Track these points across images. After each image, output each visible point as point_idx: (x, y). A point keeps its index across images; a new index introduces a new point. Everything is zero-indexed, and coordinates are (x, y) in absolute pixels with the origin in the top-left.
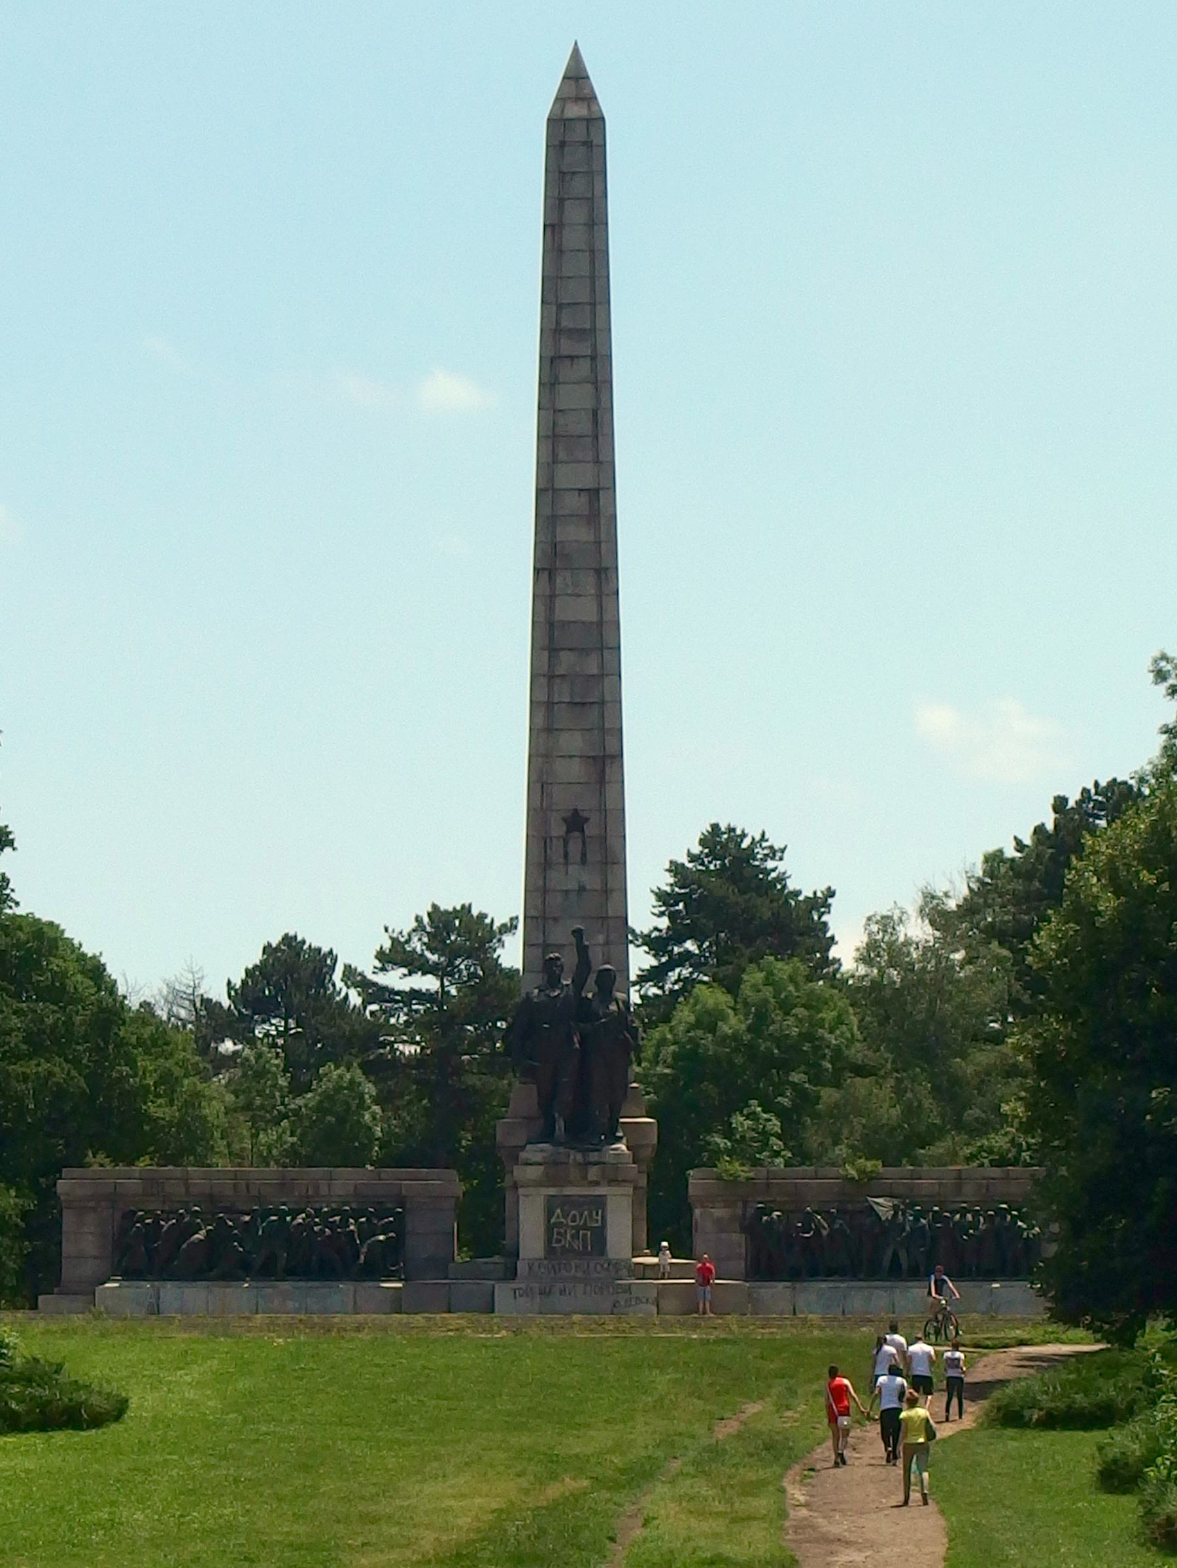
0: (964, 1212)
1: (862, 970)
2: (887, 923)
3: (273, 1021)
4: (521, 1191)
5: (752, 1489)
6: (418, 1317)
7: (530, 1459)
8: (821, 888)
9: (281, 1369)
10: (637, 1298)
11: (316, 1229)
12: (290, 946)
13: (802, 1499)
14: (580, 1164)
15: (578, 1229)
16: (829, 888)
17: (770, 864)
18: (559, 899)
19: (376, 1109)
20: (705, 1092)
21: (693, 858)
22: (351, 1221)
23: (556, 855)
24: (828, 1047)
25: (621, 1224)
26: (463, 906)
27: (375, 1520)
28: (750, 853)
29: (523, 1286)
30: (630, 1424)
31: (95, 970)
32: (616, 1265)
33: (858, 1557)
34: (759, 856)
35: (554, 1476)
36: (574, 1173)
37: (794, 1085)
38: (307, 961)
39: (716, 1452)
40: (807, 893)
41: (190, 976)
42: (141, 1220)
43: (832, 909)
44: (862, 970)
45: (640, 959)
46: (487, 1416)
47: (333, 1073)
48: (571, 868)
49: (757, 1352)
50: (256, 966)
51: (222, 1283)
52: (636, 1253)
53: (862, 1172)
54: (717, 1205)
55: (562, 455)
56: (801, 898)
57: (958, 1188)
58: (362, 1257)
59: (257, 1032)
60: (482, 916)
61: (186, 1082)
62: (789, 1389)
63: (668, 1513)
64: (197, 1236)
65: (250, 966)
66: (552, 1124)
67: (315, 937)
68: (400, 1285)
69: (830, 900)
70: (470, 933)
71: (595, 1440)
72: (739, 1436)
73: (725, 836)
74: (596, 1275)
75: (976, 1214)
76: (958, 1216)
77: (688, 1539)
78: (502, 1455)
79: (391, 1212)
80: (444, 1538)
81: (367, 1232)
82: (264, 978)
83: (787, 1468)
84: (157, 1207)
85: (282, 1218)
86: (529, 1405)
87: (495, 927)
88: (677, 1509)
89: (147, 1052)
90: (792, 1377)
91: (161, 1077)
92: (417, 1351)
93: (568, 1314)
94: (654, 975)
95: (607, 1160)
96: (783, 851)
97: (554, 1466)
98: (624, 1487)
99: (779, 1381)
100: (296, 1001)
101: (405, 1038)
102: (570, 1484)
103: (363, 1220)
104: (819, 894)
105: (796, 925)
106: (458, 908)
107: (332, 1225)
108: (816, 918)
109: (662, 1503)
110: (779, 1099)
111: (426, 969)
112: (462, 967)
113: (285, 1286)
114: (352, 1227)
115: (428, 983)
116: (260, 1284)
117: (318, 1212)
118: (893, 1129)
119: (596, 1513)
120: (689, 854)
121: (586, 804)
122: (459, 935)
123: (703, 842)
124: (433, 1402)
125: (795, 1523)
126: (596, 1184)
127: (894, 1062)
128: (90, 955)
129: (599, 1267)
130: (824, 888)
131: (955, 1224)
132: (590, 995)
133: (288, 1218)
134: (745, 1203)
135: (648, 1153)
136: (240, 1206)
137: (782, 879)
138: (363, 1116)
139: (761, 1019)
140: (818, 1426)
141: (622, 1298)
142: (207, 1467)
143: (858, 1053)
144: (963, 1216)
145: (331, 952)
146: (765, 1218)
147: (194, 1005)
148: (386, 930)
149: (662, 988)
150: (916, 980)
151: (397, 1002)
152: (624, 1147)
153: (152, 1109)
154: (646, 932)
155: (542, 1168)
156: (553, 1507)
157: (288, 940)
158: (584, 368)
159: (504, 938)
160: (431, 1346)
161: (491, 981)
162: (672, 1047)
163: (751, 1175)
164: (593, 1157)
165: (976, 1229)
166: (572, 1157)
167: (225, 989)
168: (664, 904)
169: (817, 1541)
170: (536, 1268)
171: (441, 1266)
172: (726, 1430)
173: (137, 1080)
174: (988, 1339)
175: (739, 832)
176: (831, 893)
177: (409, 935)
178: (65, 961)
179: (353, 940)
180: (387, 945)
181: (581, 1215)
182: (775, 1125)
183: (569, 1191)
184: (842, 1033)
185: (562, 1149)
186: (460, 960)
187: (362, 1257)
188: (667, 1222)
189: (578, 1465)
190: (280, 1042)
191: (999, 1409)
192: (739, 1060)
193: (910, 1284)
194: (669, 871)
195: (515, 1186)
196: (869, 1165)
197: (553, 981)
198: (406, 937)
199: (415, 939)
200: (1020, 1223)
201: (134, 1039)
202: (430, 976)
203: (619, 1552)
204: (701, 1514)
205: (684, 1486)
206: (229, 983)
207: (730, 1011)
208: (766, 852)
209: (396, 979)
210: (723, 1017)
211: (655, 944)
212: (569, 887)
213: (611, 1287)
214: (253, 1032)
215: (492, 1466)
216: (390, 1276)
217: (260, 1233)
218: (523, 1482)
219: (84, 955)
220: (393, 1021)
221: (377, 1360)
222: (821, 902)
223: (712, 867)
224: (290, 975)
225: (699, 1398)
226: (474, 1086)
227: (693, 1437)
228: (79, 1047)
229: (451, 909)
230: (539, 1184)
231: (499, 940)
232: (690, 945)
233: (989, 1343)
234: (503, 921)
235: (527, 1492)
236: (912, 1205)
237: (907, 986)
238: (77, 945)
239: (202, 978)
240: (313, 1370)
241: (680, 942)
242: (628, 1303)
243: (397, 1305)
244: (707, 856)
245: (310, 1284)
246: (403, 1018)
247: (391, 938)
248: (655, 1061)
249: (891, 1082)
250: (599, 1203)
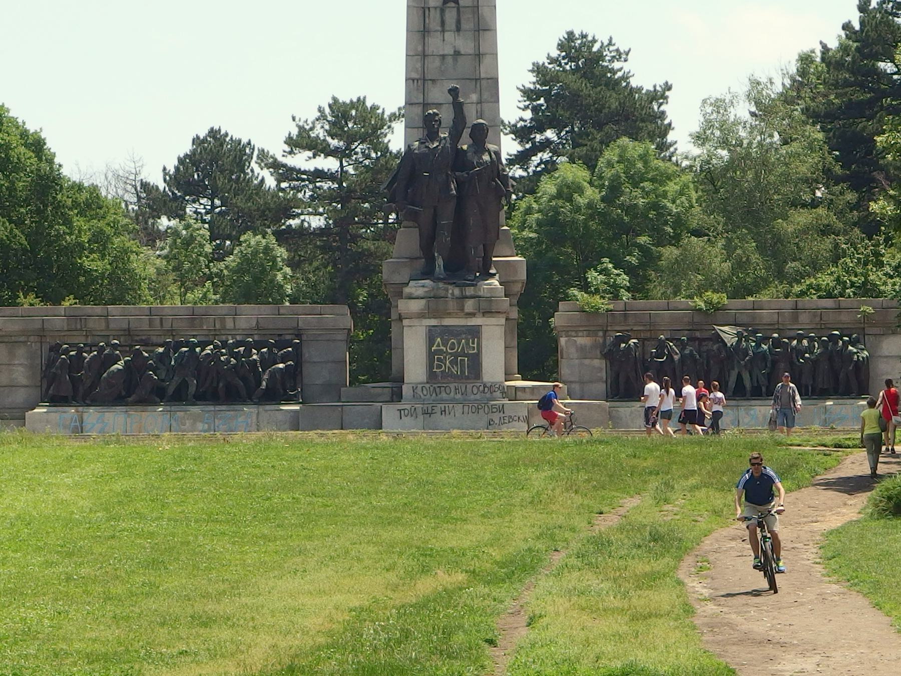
0: (800, 338)
1: (696, 151)
2: (719, 105)
3: (202, 201)
4: (406, 322)
5: (652, 580)
6: (311, 433)
7: (401, 554)
8: (660, 82)
9: (161, 471)
10: (510, 417)
11: (222, 358)
12: (214, 138)
13: (706, 592)
15: (456, 355)
16: (667, 83)
17: (616, 65)
18: (438, 62)
19: (288, 270)
20: (565, 250)
21: (553, 61)
22: (254, 351)
23: (434, 24)
24: (670, 215)
25: (495, 353)
26: (359, 99)
27: (206, 622)
28: (600, 56)
29: (408, 407)
30: (507, 519)
31: (37, 145)
32: (491, 388)
33: (809, 664)
34: (607, 58)
35: (425, 570)
36: (452, 305)
37: (640, 247)
38: (230, 150)
39: (601, 544)
40: (648, 86)
41: (132, 165)
42: (66, 352)
43: (669, 100)
44: (696, 151)
45: (509, 146)
46: (361, 512)
47: (251, 239)
48: (446, 34)
49: (630, 451)
50: (186, 156)
51: (139, 408)
52: (508, 376)
53: (709, 303)
54: (580, 334)
56: (644, 92)
57: (795, 319)
58: (264, 383)
59: (188, 210)
60: (375, 108)
61: (116, 241)
62: (667, 484)
63: (558, 612)
64: (116, 366)
65: (182, 156)
66: (431, 261)
67: (237, 130)
68: (297, 407)
69: (667, 93)
70: (364, 121)
71: (469, 535)
72: (621, 529)
73: (579, 42)
74: (473, 397)
75: (811, 340)
76: (795, 342)
77: (587, 643)
78: (372, 549)
79: (289, 344)
80: (283, 644)
81: (267, 362)
82: (193, 165)
83: (680, 559)
84: (81, 341)
85: (192, 350)
86: (405, 501)
87: (385, 116)
88: (567, 605)
89: (81, 214)
90: (667, 473)
91: (94, 235)
92: (298, 454)
93: (448, 430)
94: (522, 159)
95: (481, 293)
96: (627, 54)
97: (426, 559)
98: (503, 581)
99: (654, 477)
100: (220, 184)
101: (310, 210)
102: (444, 578)
103: (265, 350)
104: (658, 88)
105: (640, 115)
106: (355, 100)
107: (237, 356)
108: (656, 107)
109: (549, 598)
110: (628, 257)
111: (329, 152)
112: (358, 150)
113: (195, 410)
114: (255, 357)
115: (330, 164)
116: (173, 408)
117: (225, 344)
118: (724, 281)
119: (472, 610)
120: (549, 57)
122: (355, 124)
123: (561, 47)
124: (308, 499)
125: (706, 620)
126: (472, 315)
127: (725, 224)
128: (31, 132)
129: (475, 391)
130: (662, 83)
131: (792, 349)
132: (465, 147)
133: (198, 350)
134: (605, 332)
135: (518, 288)
136: (155, 339)
137: (625, 78)
138: (276, 275)
139: (613, 191)
140: (699, 519)
141: (496, 417)
142: (49, 564)
143: (697, 217)
144: (800, 342)
145: (249, 143)
146: (623, 345)
147: (136, 189)
148: (294, 119)
149: (526, 170)
150: (741, 159)
151: (303, 180)
152: (497, 283)
153: (86, 263)
154: (513, 122)
155: (423, 302)
156: (422, 605)
157: (213, 133)
159: (393, 124)
160: (312, 450)
161: (382, 161)
162: (536, 215)
163: (611, 307)
164: (470, 291)
165: (811, 353)
166: (450, 291)
167: (161, 174)
168: (528, 100)
169: (740, 642)
170: (419, 391)
171: (333, 390)
172: (607, 523)
173: (74, 237)
174: (846, 439)
175: (590, 38)
176: (668, 87)
177: (313, 123)
178: (9, 135)
179: (265, 126)
180: (295, 132)
181: (459, 344)
182: (624, 279)
183: (448, 322)
184: (683, 203)
185: (441, 285)
186: (356, 144)
187: (264, 383)
188: (536, 355)
189: (454, 559)
190: (208, 218)
191: (890, 498)
192: (593, 225)
193: (753, 402)
194: (532, 71)
195: (400, 319)
196: (715, 297)
197: (432, 134)
198: (311, 125)
199: (318, 126)
200: (850, 348)
201: (69, 202)
202: (330, 158)
203: (499, 661)
204: (595, 611)
205: (572, 579)
206: (165, 169)
207: (585, 184)
208: (613, 54)
209: (302, 161)
210: (580, 190)
211: (521, 133)
212: (446, 52)
213: (487, 406)
214: (184, 210)
215: (359, 560)
216: (289, 400)
217: (173, 363)
218: (392, 577)
219: (26, 131)
220: (300, 195)
221: (258, 461)
222: (660, 95)
223: (568, 67)
224: (214, 164)
225: (576, 492)
226: (369, 250)
227: (573, 530)
228: (22, 210)
229: (348, 102)
230: (421, 316)
231: (389, 127)
232: (550, 134)
233: (850, 443)
234: (393, 111)
235: (395, 588)
236: (755, 332)
237: (731, 166)
238: (21, 124)
239: (142, 166)
240: (192, 471)
241: (542, 130)
242: (502, 423)
243: (295, 423)
244: (564, 58)
245: (218, 408)
246: (308, 194)
247: (298, 126)
248: (522, 228)
249: (721, 243)
250: (475, 333)
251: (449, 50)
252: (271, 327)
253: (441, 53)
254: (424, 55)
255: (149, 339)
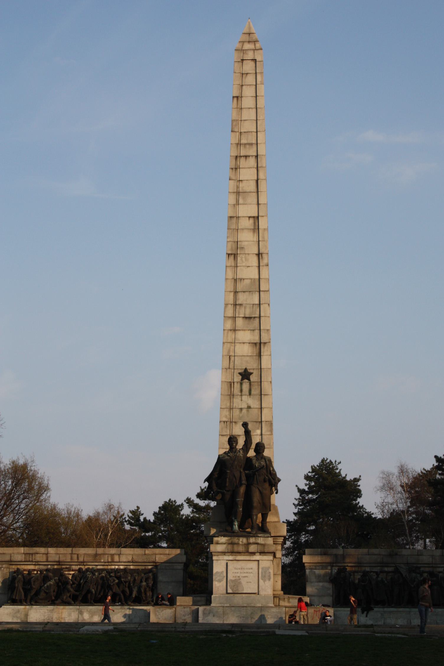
14: (245, 544)
18: (238, 411)
23: (236, 390)
54: (318, 568)
55: (241, 201)
65: (157, 510)
121: (252, 365)
126: (253, 554)
155: (225, 546)
158: (252, 162)
159: (136, 508)
164: (252, 540)
176: (360, 476)
209: (202, 503)
212: (243, 407)
230: (224, 553)
251: (244, 406)
252: (140, 561)
253: (240, 407)
254: (231, 409)
255: (70, 567)
